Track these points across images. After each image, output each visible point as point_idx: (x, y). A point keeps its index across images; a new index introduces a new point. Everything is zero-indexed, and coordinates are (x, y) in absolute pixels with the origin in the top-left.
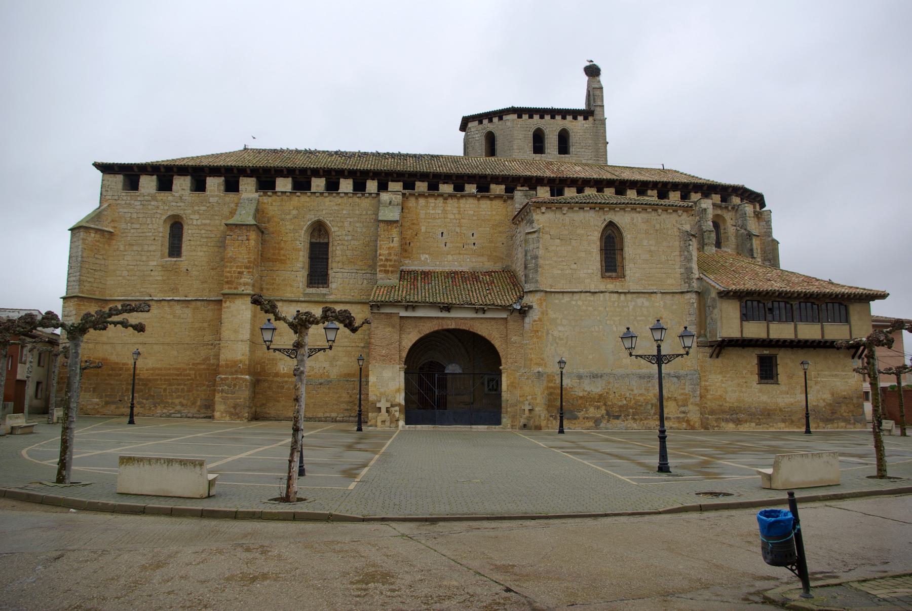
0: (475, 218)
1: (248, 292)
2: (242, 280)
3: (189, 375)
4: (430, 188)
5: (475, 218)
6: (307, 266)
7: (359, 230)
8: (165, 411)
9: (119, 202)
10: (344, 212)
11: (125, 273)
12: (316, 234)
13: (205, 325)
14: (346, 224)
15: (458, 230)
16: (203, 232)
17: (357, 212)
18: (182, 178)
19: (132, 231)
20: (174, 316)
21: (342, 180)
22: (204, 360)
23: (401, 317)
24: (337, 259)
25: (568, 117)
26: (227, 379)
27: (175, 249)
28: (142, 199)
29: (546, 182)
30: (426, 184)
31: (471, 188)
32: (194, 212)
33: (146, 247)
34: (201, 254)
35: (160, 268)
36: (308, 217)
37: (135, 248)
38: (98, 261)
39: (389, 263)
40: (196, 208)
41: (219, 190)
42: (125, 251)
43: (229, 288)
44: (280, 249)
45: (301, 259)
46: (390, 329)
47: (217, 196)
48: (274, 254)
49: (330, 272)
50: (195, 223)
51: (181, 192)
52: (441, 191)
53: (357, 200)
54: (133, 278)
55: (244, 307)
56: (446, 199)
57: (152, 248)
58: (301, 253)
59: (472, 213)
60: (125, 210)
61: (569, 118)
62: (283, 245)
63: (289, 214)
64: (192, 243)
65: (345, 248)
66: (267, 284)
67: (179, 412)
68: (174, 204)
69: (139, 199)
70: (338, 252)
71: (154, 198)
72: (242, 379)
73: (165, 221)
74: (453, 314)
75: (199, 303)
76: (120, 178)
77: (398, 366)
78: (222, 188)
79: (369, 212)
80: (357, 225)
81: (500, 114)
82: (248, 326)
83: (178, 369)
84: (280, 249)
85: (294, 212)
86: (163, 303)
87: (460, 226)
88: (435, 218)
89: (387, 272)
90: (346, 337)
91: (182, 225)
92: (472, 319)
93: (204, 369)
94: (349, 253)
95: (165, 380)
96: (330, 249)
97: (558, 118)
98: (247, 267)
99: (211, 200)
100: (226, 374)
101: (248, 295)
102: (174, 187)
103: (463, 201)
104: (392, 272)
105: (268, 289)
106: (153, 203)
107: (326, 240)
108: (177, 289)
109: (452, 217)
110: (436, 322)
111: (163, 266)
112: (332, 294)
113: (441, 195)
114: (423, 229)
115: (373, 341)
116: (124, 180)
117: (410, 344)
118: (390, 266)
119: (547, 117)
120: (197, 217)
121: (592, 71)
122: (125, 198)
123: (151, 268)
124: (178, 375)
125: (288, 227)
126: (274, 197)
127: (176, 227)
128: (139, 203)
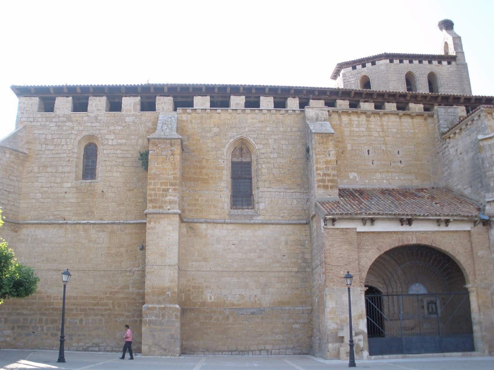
0: (399, 136)
1: (175, 211)
2: (168, 198)
3: (106, 305)
4: (352, 106)
5: (399, 136)
6: (230, 187)
7: (284, 147)
8: (82, 344)
9: (34, 124)
10: (268, 129)
11: (39, 195)
12: (238, 153)
13: (123, 250)
14: (271, 141)
15: (383, 147)
16: (119, 152)
17: (281, 129)
18: (98, 98)
19: (47, 152)
20: (90, 241)
21: (262, 98)
22: (122, 288)
23: (358, 232)
24: (263, 178)
25: (433, 62)
26: (154, 308)
27: (89, 171)
28: (57, 120)
29: (462, 101)
30: (347, 103)
31: (391, 107)
32: (110, 132)
33: (60, 169)
34: (118, 174)
35: (74, 190)
36: (230, 134)
37: (49, 170)
38: (11, 183)
39: (327, 178)
40: (112, 128)
41: (135, 110)
42: (39, 173)
43: (154, 207)
44: (202, 168)
45: (224, 178)
46: (347, 246)
47: (133, 115)
48: (195, 173)
49: (255, 192)
50: (110, 143)
51: (96, 113)
52: (362, 109)
53: (281, 117)
54: (46, 201)
55: (170, 228)
56: (368, 116)
57: (67, 169)
58: (225, 172)
59: (395, 130)
60: (41, 132)
61: (435, 63)
62: (204, 163)
63: (210, 131)
64: (108, 163)
65: (271, 166)
66: (189, 205)
67: (97, 345)
68: (89, 124)
69: (54, 120)
70: (265, 171)
71: (69, 119)
72: (171, 308)
73: (79, 142)
74: (416, 227)
75: (115, 227)
76: (36, 100)
77: (359, 289)
78: (139, 107)
79: (294, 129)
80: (283, 142)
81: (373, 60)
82: (175, 249)
83: (95, 298)
84: (202, 168)
85: (216, 130)
86: (77, 226)
87: (385, 144)
88: (359, 136)
89: (326, 187)
90: (277, 262)
91: (96, 146)
92: (434, 232)
93: (122, 298)
94: (275, 171)
95: (82, 310)
96: (253, 169)
97: (425, 62)
98: (172, 184)
100: (153, 303)
101: (175, 214)
102: (89, 108)
103: (385, 119)
104: (332, 187)
105: (190, 211)
106: (67, 124)
107: (248, 160)
108: (92, 212)
109: (377, 135)
110: (395, 237)
111: (77, 188)
112: (259, 215)
113: (364, 113)
114: (349, 147)
115: (328, 260)
116: (40, 103)
117: (370, 263)
118: (329, 181)
119: (416, 62)
120: (113, 137)
121: (447, 25)
122: (40, 120)
123: (65, 190)
124: (95, 305)
125: (210, 145)
126: (194, 115)
127: (90, 153)
128: (54, 124)
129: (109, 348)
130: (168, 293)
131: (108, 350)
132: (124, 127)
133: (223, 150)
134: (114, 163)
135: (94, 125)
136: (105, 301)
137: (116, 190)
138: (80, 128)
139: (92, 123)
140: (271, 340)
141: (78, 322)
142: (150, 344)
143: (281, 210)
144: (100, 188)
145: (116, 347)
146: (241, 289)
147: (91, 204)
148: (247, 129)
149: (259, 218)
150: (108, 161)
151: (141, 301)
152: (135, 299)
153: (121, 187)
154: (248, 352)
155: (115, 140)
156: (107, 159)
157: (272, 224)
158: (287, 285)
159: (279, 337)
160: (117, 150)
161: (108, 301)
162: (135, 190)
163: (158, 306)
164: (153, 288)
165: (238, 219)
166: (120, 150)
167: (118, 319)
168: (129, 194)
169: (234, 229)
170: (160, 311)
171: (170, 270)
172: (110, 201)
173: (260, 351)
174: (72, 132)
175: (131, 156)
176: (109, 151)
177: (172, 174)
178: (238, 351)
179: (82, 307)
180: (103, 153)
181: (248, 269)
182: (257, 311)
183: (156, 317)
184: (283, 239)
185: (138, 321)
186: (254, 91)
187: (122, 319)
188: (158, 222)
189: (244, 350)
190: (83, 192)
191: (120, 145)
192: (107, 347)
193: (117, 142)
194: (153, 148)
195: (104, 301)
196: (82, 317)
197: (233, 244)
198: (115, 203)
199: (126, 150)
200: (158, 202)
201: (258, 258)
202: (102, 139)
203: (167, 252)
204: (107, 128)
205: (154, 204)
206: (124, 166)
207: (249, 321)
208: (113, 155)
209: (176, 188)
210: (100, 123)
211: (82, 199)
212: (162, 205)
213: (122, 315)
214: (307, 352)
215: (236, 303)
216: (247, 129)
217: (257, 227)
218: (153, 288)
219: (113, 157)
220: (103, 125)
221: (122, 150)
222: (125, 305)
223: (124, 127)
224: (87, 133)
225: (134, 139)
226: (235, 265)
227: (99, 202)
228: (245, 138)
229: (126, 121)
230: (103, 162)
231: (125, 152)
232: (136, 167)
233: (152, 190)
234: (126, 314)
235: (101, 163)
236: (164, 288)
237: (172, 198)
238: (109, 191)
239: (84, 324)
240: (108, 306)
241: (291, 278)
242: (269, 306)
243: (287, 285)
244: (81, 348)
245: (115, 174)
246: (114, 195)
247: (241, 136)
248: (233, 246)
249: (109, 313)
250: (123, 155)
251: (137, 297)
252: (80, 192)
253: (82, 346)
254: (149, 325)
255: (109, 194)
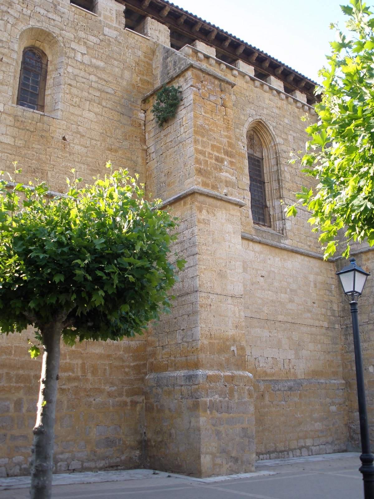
16: (93, 78)
32: (79, 40)
34: (91, 116)
40: (82, 34)
55: (229, 227)
64: (74, 91)
68: (42, 12)
72: (242, 377)
93: (100, 357)
95: (19, 378)
99: (106, 30)
100: (211, 367)
112: (286, 238)
129: (75, 464)
130: (233, 348)
131: (73, 468)
132: (101, 41)
133: (242, 129)
134: (85, 94)
135: (50, 15)
136: (68, 361)
137: (88, 143)
138: (25, 10)
139: (48, 11)
140: (311, 431)
141: (12, 406)
142: (214, 450)
143: (308, 236)
144: (60, 131)
145: (89, 460)
146: (274, 350)
147: (43, 157)
148: (265, 112)
149: (287, 242)
150: (75, 87)
151: (132, 364)
152: (121, 359)
153: (96, 140)
154: (287, 451)
155: (86, 56)
156: (73, 83)
157: (302, 254)
158: (319, 346)
159: (318, 426)
160: (90, 74)
161: (75, 362)
162: (120, 152)
163: (222, 374)
164: (211, 338)
165: (265, 238)
166: (95, 75)
167: (92, 399)
168: (110, 155)
169: (261, 253)
170: (226, 384)
171: (235, 305)
172: (77, 160)
173: (300, 448)
174: (9, 10)
175: (113, 92)
176: (77, 72)
177: (226, 136)
178: (276, 452)
179: (21, 372)
180: (66, 69)
181: (280, 318)
182: (295, 387)
183: (220, 396)
184: (312, 278)
185: (129, 404)
186: (267, 64)
187: (99, 399)
188: (213, 213)
189: (283, 449)
190: (28, 130)
191: (95, 67)
192: (73, 462)
193: (91, 62)
194: (197, 84)
195: (65, 361)
196: (21, 394)
197: (261, 276)
198: (86, 166)
199: (105, 81)
200: (211, 177)
201: (290, 302)
202: (64, 45)
203: (228, 271)
204: (73, 30)
205: (205, 179)
206: (102, 105)
207: (286, 401)
208: (84, 80)
209: (233, 162)
210: (62, 17)
211: (26, 141)
212: (216, 185)
213: (100, 391)
214: (344, 448)
215: (269, 371)
216: (265, 112)
217: (285, 254)
218: (211, 338)
219: (84, 83)
220: (68, 24)
221: (99, 78)
222: (105, 369)
223: (101, 41)
224: (38, 25)
225: (117, 67)
226: (265, 309)
227: (58, 157)
228: (264, 122)
229: (105, 33)
230: (66, 85)
231: (104, 83)
232: (121, 114)
233: (200, 153)
234: (108, 388)
235: (63, 86)
236: (227, 340)
237: (230, 176)
238: (76, 141)
239: (24, 410)
240: (73, 372)
241: (322, 337)
242: (303, 378)
243: (319, 346)
244: (17, 470)
245: (86, 114)
246: (84, 150)
247: (260, 117)
248: (262, 278)
249: (76, 387)
250: (100, 86)
251: (126, 355)
252: (22, 127)
253: (19, 464)
254: (211, 413)
255: (76, 147)
